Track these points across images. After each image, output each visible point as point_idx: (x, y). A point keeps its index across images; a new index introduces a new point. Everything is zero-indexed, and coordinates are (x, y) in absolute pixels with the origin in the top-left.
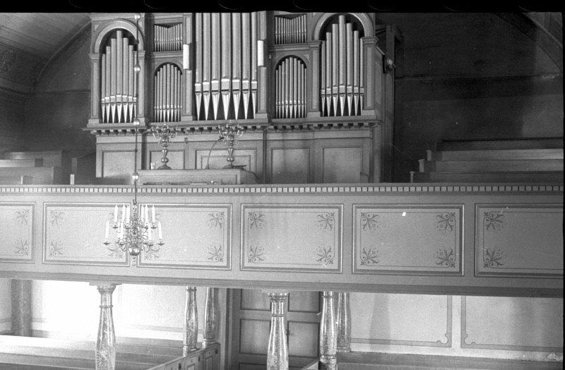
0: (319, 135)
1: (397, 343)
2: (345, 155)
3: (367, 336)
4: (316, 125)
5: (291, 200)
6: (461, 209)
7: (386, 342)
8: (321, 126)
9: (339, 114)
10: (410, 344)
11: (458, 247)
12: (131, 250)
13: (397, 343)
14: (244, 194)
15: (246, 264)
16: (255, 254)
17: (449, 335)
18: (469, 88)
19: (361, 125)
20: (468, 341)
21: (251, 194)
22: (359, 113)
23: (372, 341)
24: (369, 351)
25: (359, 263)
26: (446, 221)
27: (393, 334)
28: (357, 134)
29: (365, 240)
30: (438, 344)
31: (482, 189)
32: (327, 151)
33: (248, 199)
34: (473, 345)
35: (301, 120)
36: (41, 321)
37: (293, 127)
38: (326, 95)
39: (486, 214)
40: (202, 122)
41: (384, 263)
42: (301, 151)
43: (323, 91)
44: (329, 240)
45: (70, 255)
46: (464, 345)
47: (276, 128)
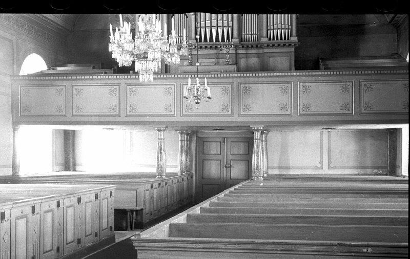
0: (266, 50)
1: (294, 168)
2: (282, 60)
3: (276, 165)
4: (266, 45)
5: (264, 79)
6: (352, 82)
7: (288, 168)
8: (268, 45)
9: (277, 39)
10: (301, 168)
11: (351, 101)
12: (196, 101)
13: (294, 168)
14: (240, 77)
15: (242, 113)
16: (247, 108)
17: (321, 163)
18: (332, 31)
19: (290, 45)
20: (332, 165)
21: (244, 77)
22: (288, 39)
23: (280, 168)
24: (279, 173)
25: (301, 110)
26: (345, 89)
27: (291, 164)
28: (287, 50)
29: (304, 99)
30: (316, 168)
31: (360, 72)
32: (271, 59)
33: (243, 80)
34: (335, 168)
35: (257, 42)
36: (81, 165)
37: (252, 46)
38: (270, 29)
39: (365, 85)
40: (201, 43)
41: (314, 109)
42: (256, 59)
43: (269, 28)
44: (286, 99)
45: (140, 111)
46: (329, 168)
47: (243, 47)
